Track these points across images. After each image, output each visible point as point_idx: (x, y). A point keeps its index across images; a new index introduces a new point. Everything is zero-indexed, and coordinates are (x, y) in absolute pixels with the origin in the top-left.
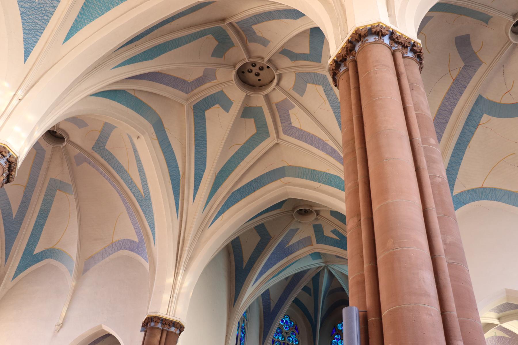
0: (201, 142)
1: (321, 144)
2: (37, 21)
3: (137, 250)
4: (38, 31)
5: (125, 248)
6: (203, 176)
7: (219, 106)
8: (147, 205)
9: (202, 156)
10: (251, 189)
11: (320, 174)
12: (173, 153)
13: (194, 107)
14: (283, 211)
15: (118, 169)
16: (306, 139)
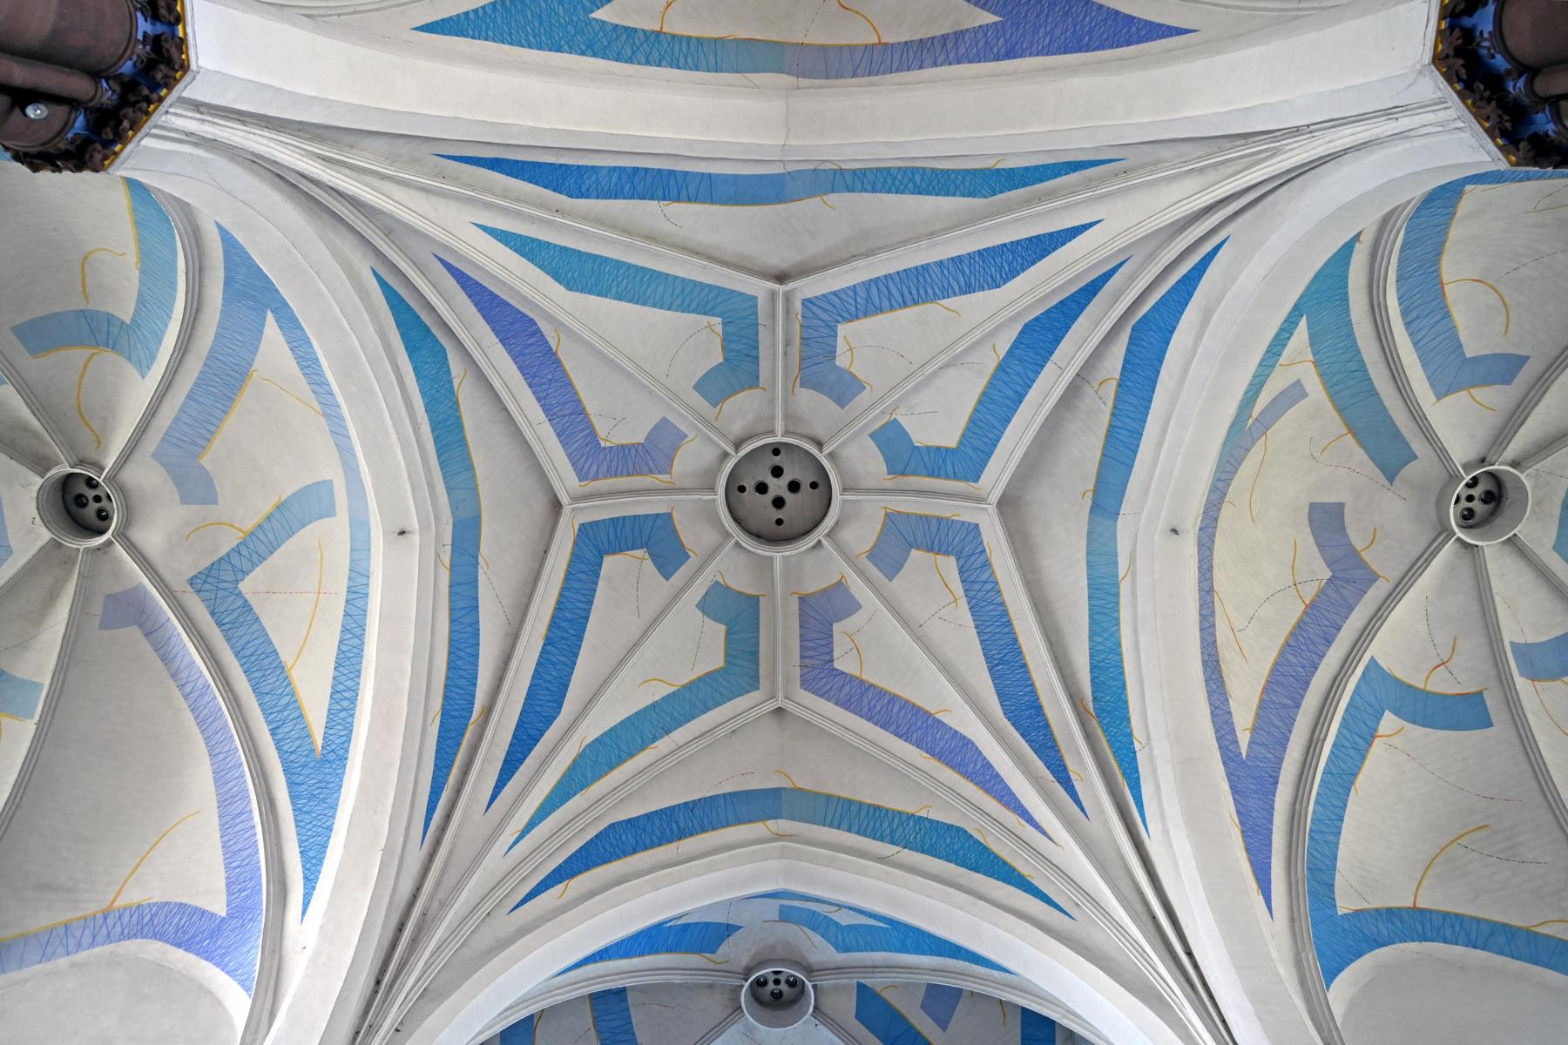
0: (565, 635)
1: (919, 723)
5: (158, 936)
6: (542, 735)
7: (647, 556)
8: (320, 782)
9: (555, 678)
10: (671, 829)
11: (897, 820)
12: (476, 635)
13: (579, 529)
14: (718, 967)
15: (253, 658)
16: (869, 710)
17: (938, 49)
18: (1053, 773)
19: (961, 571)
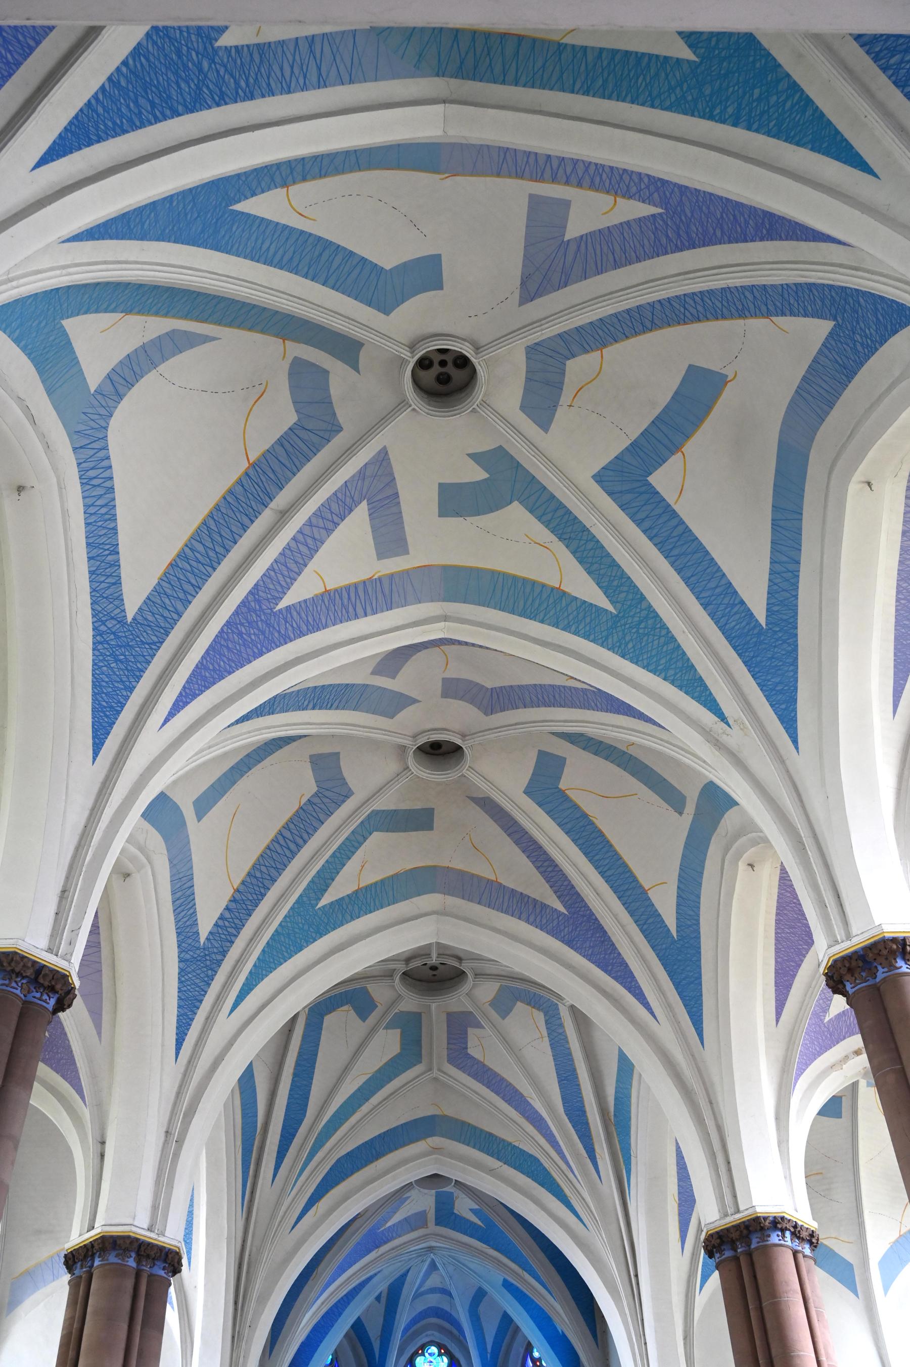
2: (197, 981)
4: (196, 999)
6: (297, 1132)
7: (351, 1008)
17: (531, 907)
18: (587, 1152)
19: (547, 1022)
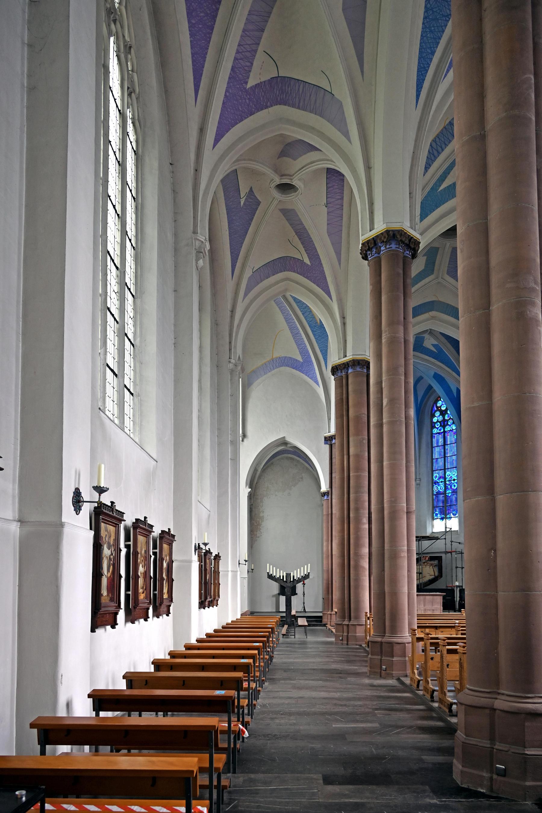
3: (300, 368)
